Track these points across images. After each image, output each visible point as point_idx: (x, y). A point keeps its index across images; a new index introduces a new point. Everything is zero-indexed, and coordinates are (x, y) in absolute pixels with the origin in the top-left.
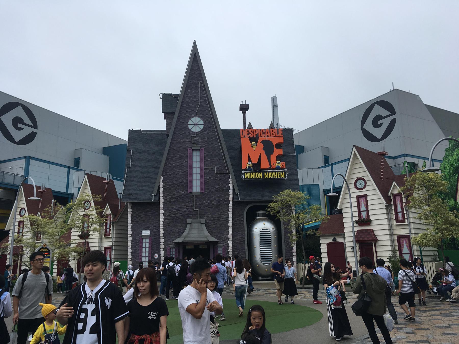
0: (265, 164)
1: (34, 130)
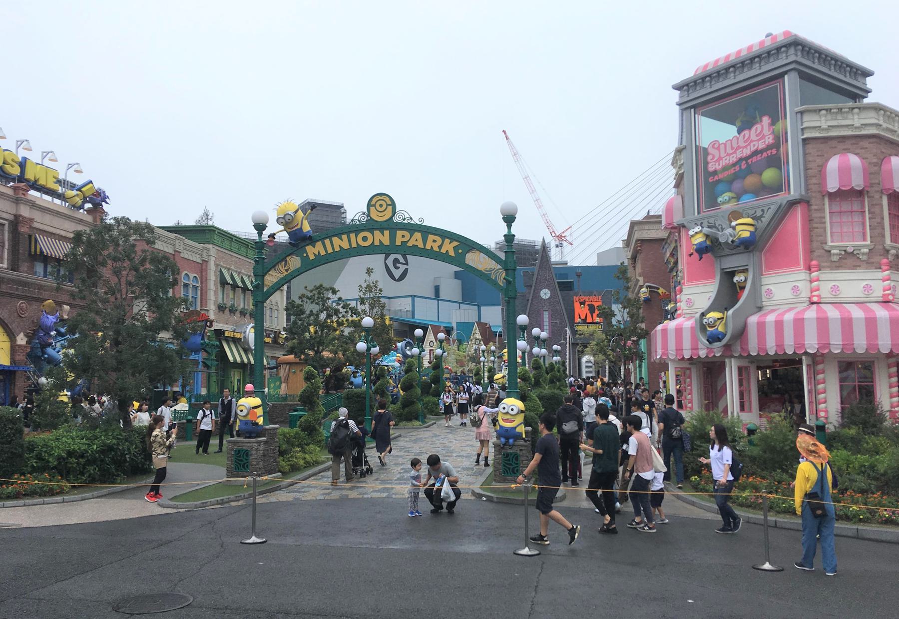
0: (589, 320)
1: (406, 267)
